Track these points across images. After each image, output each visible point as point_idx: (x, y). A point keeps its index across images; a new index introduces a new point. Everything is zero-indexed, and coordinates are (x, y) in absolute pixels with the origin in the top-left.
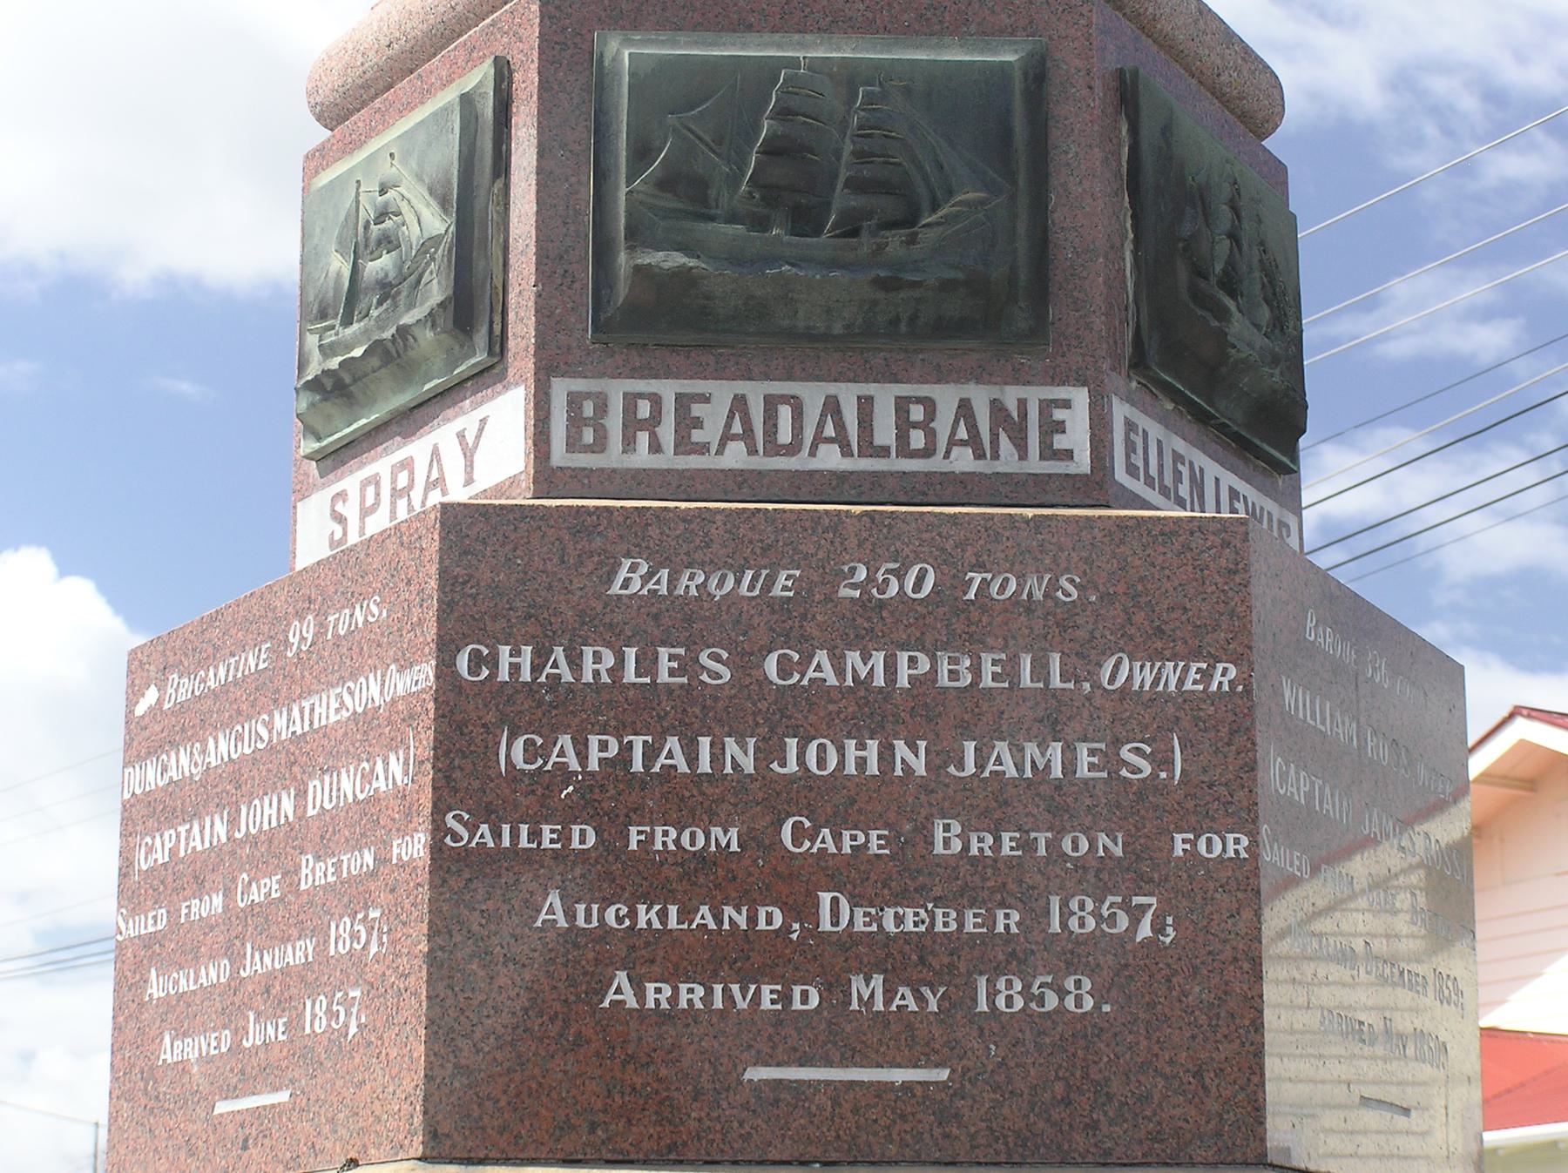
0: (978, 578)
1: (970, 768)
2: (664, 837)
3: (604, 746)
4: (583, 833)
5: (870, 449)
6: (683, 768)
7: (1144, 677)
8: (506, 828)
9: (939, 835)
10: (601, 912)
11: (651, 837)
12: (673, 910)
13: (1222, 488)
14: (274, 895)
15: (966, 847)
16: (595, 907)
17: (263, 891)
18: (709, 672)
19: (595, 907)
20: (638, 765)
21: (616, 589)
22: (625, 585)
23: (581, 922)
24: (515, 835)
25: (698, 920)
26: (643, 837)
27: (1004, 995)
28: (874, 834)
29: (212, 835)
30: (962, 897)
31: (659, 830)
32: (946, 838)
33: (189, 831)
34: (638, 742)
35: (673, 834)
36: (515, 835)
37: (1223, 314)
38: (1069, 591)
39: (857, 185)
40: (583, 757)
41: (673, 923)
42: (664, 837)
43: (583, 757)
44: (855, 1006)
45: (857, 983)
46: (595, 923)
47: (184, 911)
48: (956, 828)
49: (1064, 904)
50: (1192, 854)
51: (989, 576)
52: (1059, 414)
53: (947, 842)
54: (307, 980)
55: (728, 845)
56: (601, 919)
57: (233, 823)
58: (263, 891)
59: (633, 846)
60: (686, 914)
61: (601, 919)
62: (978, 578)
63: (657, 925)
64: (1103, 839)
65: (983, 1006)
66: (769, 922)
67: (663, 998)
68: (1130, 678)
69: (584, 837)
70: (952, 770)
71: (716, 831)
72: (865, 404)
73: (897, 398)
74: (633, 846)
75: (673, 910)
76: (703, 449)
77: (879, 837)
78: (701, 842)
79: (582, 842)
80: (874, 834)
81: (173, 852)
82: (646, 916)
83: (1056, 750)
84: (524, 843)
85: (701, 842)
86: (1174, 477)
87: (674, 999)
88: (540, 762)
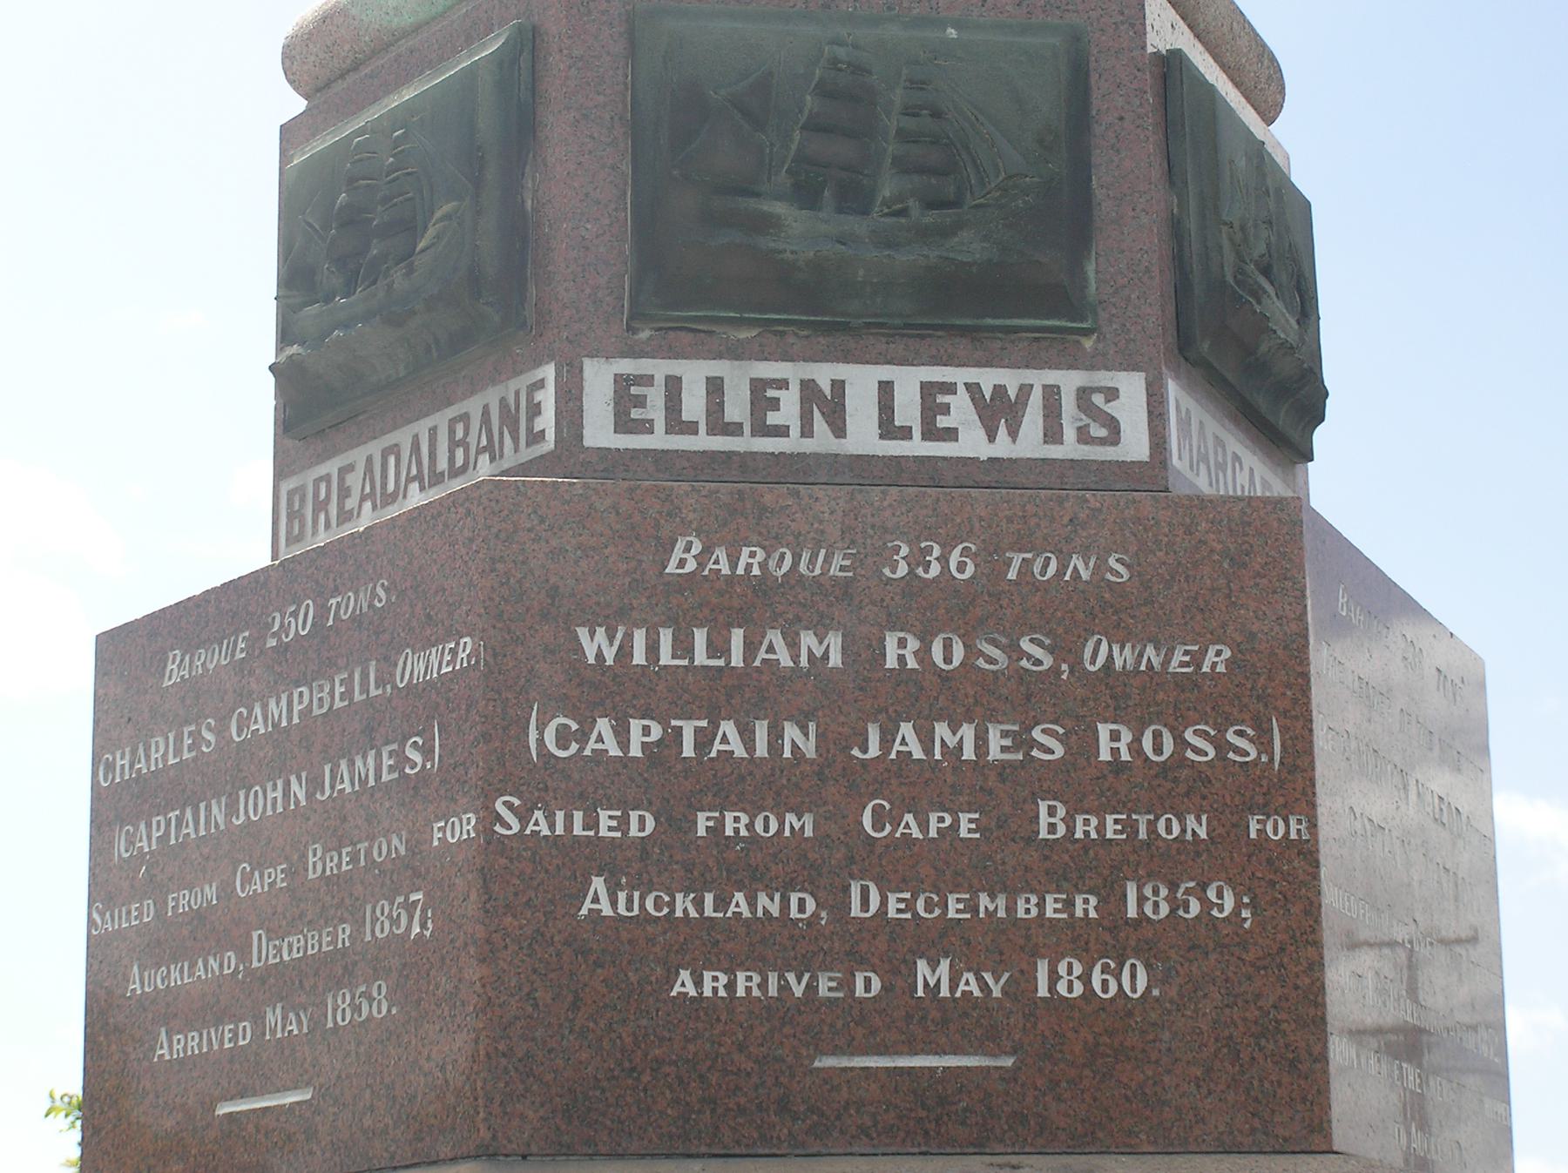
0: (1017, 559)
1: (874, 751)
2: (734, 823)
3: (646, 731)
4: (642, 819)
5: (719, 425)
6: (918, 754)
7: (1123, 658)
8: (560, 815)
9: (1044, 819)
10: (642, 899)
11: (721, 822)
12: (709, 898)
13: (1247, 472)
14: (280, 885)
15: (1071, 830)
16: (636, 895)
17: (267, 881)
18: (1029, 657)
19: (636, 895)
20: (688, 751)
21: (671, 568)
22: (682, 563)
23: (622, 910)
24: (569, 820)
25: (732, 908)
26: (711, 824)
27: (1062, 979)
28: (964, 818)
29: (207, 822)
30: (753, 881)
31: (729, 817)
32: (1049, 819)
33: (179, 820)
34: (688, 729)
35: (745, 819)
36: (569, 820)
37: (1258, 294)
38: (1117, 569)
39: (903, 166)
40: (624, 744)
41: (709, 911)
42: (734, 823)
43: (624, 744)
44: (920, 993)
45: (922, 967)
46: (636, 912)
47: (171, 904)
48: (1061, 811)
49: (1139, 889)
50: (716, 830)
51: (1029, 556)
52: (941, 399)
53: (1052, 828)
54: (337, 970)
55: (803, 827)
56: (642, 906)
57: (232, 809)
58: (267, 881)
59: (701, 832)
60: (722, 903)
61: (642, 906)
62: (1017, 559)
63: (693, 914)
64: (1191, 822)
65: (1043, 991)
66: (802, 909)
67: (754, 984)
68: (1110, 657)
69: (642, 824)
70: (856, 752)
71: (790, 818)
72: (715, 387)
73: (722, 379)
74: (701, 832)
75: (709, 898)
76: (781, 431)
77: (1116, 822)
78: (1176, 830)
79: (642, 829)
80: (964, 818)
81: (164, 839)
82: (683, 904)
83: (968, 732)
84: (578, 830)
85: (1176, 830)
86: (1213, 459)
87: (731, 986)
88: (574, 747)
